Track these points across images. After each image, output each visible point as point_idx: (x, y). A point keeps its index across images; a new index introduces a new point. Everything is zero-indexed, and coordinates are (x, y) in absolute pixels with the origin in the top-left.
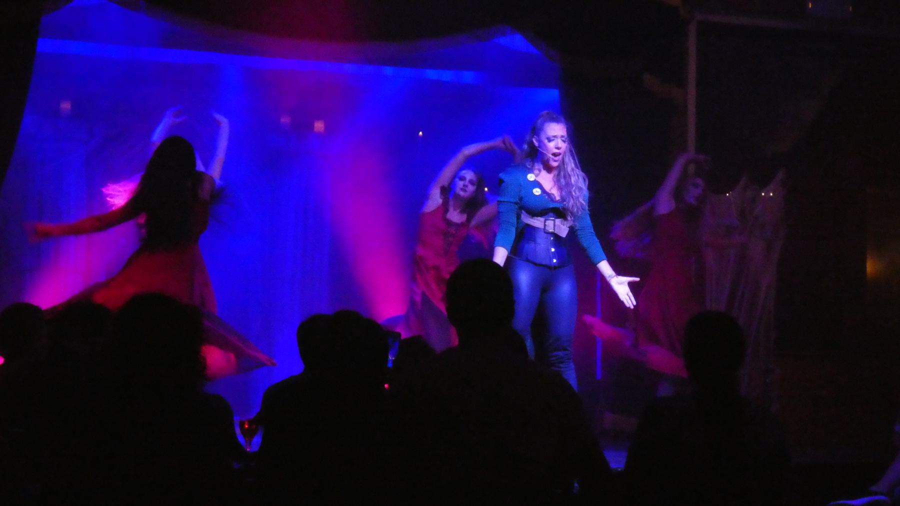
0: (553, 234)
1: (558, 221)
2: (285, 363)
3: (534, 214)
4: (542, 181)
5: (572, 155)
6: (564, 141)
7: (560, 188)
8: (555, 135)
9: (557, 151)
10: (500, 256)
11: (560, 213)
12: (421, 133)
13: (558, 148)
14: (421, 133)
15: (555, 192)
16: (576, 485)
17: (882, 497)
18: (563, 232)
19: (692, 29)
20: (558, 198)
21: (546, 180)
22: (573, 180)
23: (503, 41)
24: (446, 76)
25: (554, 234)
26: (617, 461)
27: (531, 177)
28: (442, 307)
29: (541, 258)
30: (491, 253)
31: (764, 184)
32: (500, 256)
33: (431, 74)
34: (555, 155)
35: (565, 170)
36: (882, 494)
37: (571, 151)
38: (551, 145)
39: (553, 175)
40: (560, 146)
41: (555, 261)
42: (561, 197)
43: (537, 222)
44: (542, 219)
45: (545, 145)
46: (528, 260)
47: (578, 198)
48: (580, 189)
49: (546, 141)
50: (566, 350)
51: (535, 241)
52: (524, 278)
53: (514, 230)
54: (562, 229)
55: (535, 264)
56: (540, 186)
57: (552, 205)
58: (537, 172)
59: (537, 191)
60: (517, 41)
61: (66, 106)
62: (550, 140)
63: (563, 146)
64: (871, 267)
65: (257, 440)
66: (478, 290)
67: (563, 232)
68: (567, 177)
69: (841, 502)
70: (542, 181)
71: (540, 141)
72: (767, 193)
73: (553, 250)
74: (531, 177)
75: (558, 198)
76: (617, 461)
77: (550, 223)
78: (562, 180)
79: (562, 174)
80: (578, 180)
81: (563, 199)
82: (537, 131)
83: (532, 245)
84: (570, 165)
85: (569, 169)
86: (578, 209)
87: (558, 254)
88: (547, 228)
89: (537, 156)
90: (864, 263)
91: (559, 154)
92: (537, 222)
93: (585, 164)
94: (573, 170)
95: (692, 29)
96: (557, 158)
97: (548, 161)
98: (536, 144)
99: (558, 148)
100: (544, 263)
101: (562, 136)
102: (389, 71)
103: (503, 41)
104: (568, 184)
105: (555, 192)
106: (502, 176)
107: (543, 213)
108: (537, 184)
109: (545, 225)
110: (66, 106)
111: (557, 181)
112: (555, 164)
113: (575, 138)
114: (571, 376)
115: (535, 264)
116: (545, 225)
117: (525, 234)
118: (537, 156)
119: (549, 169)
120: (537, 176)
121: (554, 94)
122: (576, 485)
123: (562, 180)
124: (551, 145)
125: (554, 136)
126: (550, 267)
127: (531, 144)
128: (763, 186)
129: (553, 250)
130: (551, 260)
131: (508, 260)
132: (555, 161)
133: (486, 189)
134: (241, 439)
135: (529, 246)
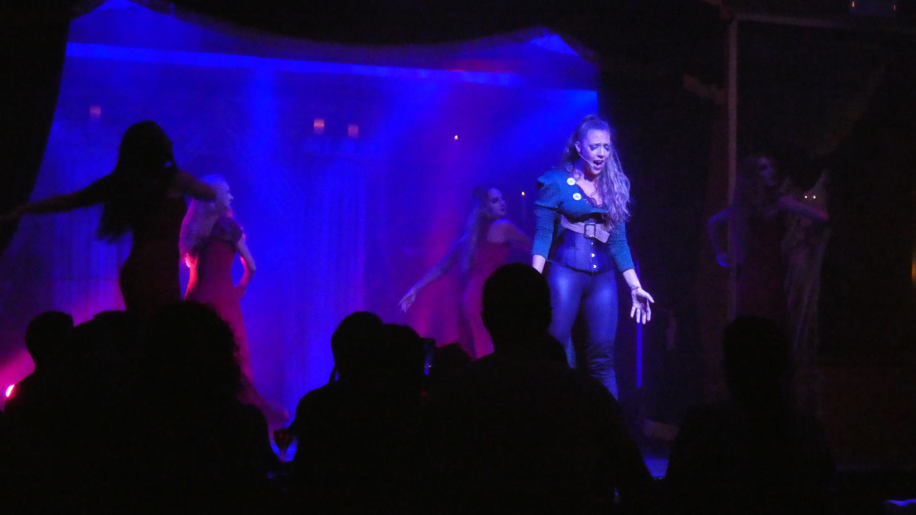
1: (598, 226)
2: (318, 369)
3: (574, 219)
4: (581, 188)
5: (616, 160)
6: (607, 149)
7: (602, 195)
8: (599, 141)
10: (539, 263)
11: (600, 218)
12: (456, 137)
13: (600, 157)
14: (456, 137)
19: (733, 30)
21: (589, 188)
22: (616, 187)
24: (482, 78)
26: (658, 470)
27: (571, 181)
29: (581, 263)
30: (530, 260)
31: (807, 187)
32: (539, 263)
33: (467, 76)
34: (596, 163)
36: (545, 207)
37: (614, 156)
38: (594, 153)
39: (595, 180)
40: (602, 154)
42: (604, 203)
44: (583, 224)
46: (567, 266)
48: (623, 196)
49: (589, 149)
51: (574, 245)
52: (564, 284)
53: (551, 236)
56: (581, 191)
57: (594, 211)
58: (577, 176)
59: (577, 197)
60: (555, 42)
61: (96, 111)
62: (592, 148)
65: (292, 450)
66: (517, 297)
67: (604, 237)
68: (610, 184)
70: (581, 188)
72: (810, 196)
73: (593, 255)
74: (571, 181)
75: (599, 201)
76: (658, 470)
77: (590, 228)
78: (605, 187)
79: (604, 180)
80: (621, 187)
81: (604, 206)
82: (580, 137)
84: (614, 170)
85: (612, 175)
86: (620, 217)
87: (598, 260)
89: (579, 162)
92: (578, 228)
94: (616, 175)
95: (733, 30)
96: (599, 166)
97: (587, 164)
98: (579, 150)
100: (584, 268)
101: (605, 145)
102: (423, 74)
103: (539, 42)
104: (610, 191)
106: (541, 180)
107: (584, 218)
109: (585, 230)
110: (96, 111)
111: (599, 188)
112: (596, 172)
113: (619, 146)
114: (611, 384)
116: (585, 230)
117: (563, 242)
118: (579, 162)
119: (589, 177)
121: (590, 96)
123: (605, 187)
124: (594, 153)
126: (590, 273)
128: (805, 190)
131: (547, 266)
132: (597, 169)
134: (276, 449)
135: (569, 253)
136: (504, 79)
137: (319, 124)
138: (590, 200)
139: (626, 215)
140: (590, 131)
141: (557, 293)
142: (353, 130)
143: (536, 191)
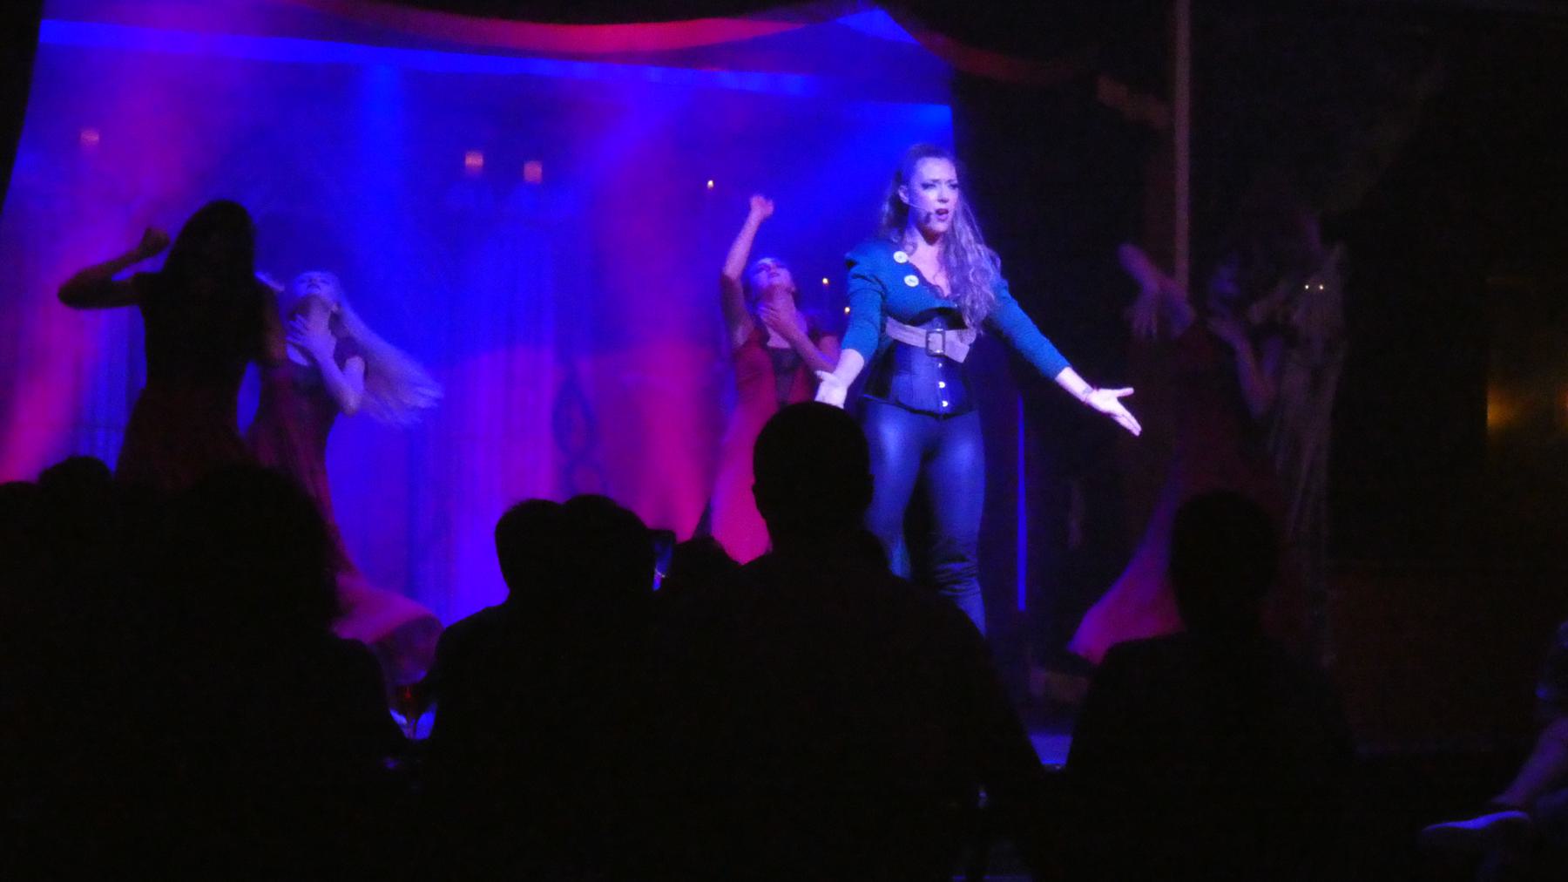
0: (942, 357)
1: (951, 335)
2: (478, 584)
4: (921, 261)
5: (969, 222)
7: (950, 272)
8: (937, 183)
9: (943, 206)
11: (952, 319)
13: (943, 201)
14: (710, 183)
15: (941, 281)
16: (983, 794)
17: (1516, 814)
18: (960, 353)
20: (947, 292)
22: (970, 258)
23: (856, 21)
25: (943, 358)
26: (1053, 752)
27: (900, 257)
28: (770, 330)
29: (924, 400)
34: (939, 212)
35: (957, 243)
38: (932, 196)
39: (936, 245)
41: (945, 404)
42: (954, 289)
43: (913, 336)
44: (921, 331)
45: (917, 195)
46: (900, 405)
47: (979, 288)
48: (985, 272)
50: (963, 560)
52: (892, 435)
54: (957, 345)
55: (913, 411)
56: (917, 272)
57: (938, 304)
59: (911, 281)
60: (878, 22)
62: (926, 186)
63: (952, 196)
64: (1495, 414)
65: (426, 721)
66: (813, 459)
67: (960, 353)
68: (961, 253)
69: (1451, 824)
71: (910, 193)
73: (942, 385)
74: (900, 257)
76: (1053, 752)
78: (952, 258)
79: (952, 249)
80: (978, 255)
82: (905, 175)
83: (906, 378)
84: (966, 235)
85: (963, 241)
87: (949, 393)
88: (931, 347)
89: (908, 219)
90: (1484, 403)
91: (946, 212)
92: (913, 336)
93: (991, 235)
98: (906, 199)
99: (943, 201)
103: (856, 21)
104: (963, 266)
105: (941, 281)
108: (911, 269)
111: (944, 261)
113: (967, 184)
114: (974, 605)
115: (913, 411)
118: (908, 219)
119: (931, 238)
120: (910, 254)
121: (938, 114)
122: (983, 794)
125: (936, 181)
126: (936, 415)
127: (896, 201)
129: (942, 385)
130: (939, 404)
133: (825, 281)
135: (900, 381)
136: (793, 83)
137: (474, 161)
138: (933, 289)
139: (990, 302)
140: (919, 162)
141: (880, 452)
142: (533, 171)
143: (842, 271)
